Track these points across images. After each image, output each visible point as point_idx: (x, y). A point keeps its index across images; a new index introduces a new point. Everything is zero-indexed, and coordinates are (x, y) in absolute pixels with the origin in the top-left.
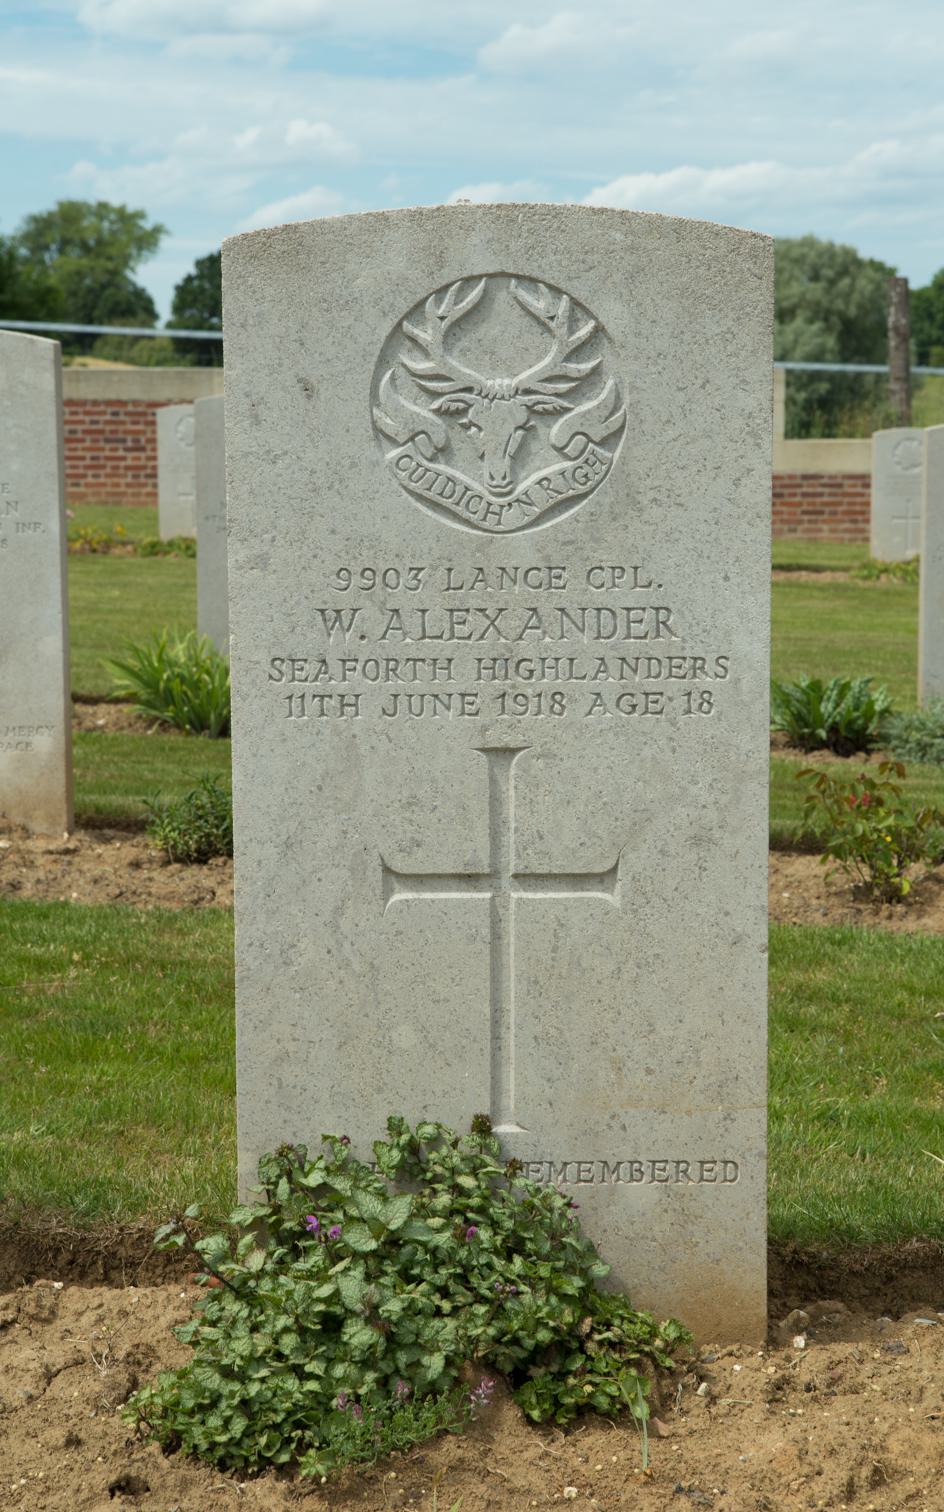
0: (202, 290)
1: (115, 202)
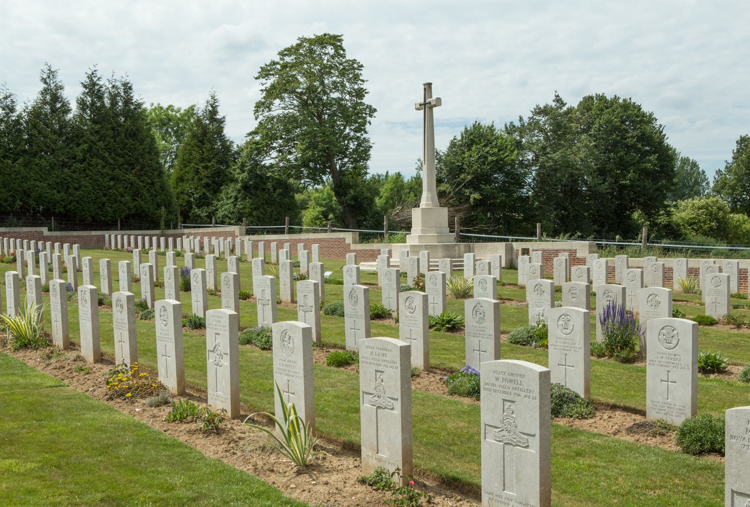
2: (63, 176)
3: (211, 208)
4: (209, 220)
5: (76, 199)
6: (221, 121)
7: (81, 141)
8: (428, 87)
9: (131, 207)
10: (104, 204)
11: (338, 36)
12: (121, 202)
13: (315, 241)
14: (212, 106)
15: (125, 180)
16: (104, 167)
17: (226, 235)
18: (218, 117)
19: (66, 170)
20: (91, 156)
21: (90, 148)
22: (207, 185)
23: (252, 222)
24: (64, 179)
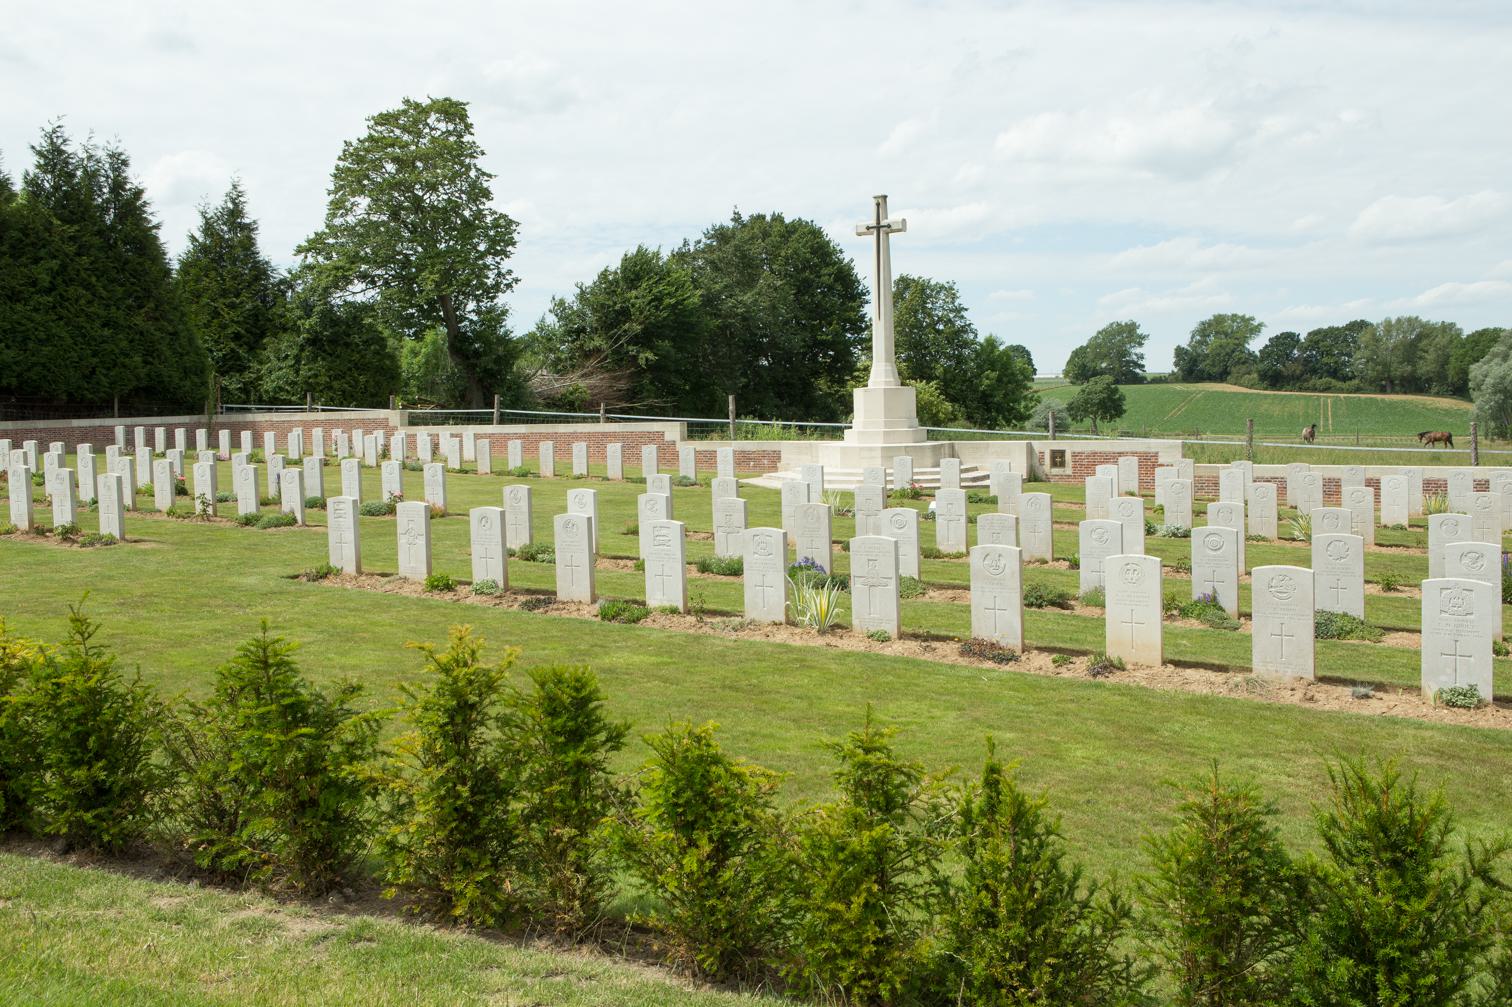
0: (1273, 352)
1: (1240, 314)
2: (15, 317)
3: (249, 376)
4: (252, 397)
5: (42, 361)
6: (249, 229)
7: (42, 253)
8: (881, 202)
9: (142, 375)
10: (93, 372)
11: (462, 104)
12: (125, 366)
13: (613, 436)
14: (233, 201)
15: (130, 327)
16: (89, 302)
17: (368, 427)
18: (246, 221)
19: (19, 307)
20: (64, 281)
21: (64, 267)
22: (237, 337)
23: (332, 399)
24: (19, 323)
